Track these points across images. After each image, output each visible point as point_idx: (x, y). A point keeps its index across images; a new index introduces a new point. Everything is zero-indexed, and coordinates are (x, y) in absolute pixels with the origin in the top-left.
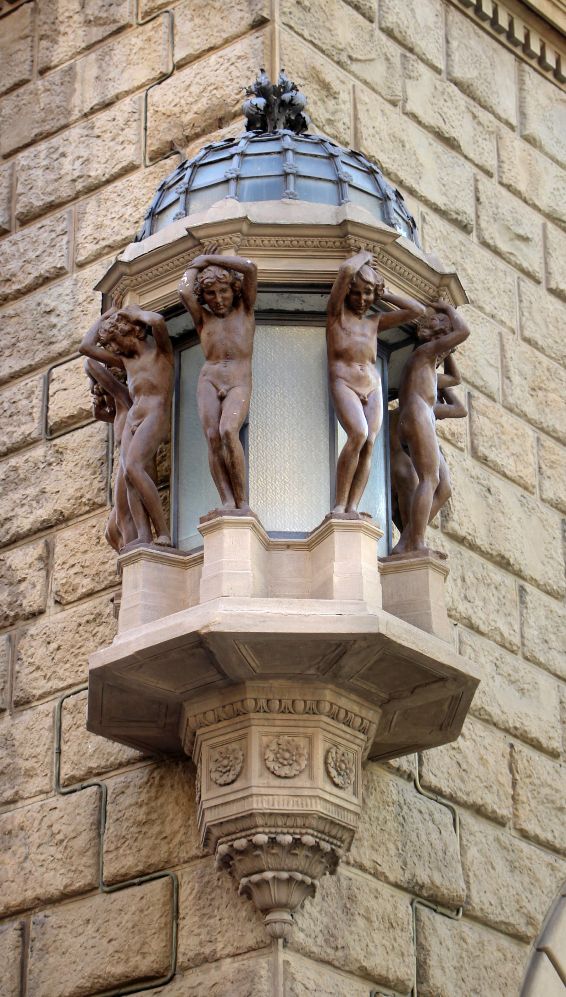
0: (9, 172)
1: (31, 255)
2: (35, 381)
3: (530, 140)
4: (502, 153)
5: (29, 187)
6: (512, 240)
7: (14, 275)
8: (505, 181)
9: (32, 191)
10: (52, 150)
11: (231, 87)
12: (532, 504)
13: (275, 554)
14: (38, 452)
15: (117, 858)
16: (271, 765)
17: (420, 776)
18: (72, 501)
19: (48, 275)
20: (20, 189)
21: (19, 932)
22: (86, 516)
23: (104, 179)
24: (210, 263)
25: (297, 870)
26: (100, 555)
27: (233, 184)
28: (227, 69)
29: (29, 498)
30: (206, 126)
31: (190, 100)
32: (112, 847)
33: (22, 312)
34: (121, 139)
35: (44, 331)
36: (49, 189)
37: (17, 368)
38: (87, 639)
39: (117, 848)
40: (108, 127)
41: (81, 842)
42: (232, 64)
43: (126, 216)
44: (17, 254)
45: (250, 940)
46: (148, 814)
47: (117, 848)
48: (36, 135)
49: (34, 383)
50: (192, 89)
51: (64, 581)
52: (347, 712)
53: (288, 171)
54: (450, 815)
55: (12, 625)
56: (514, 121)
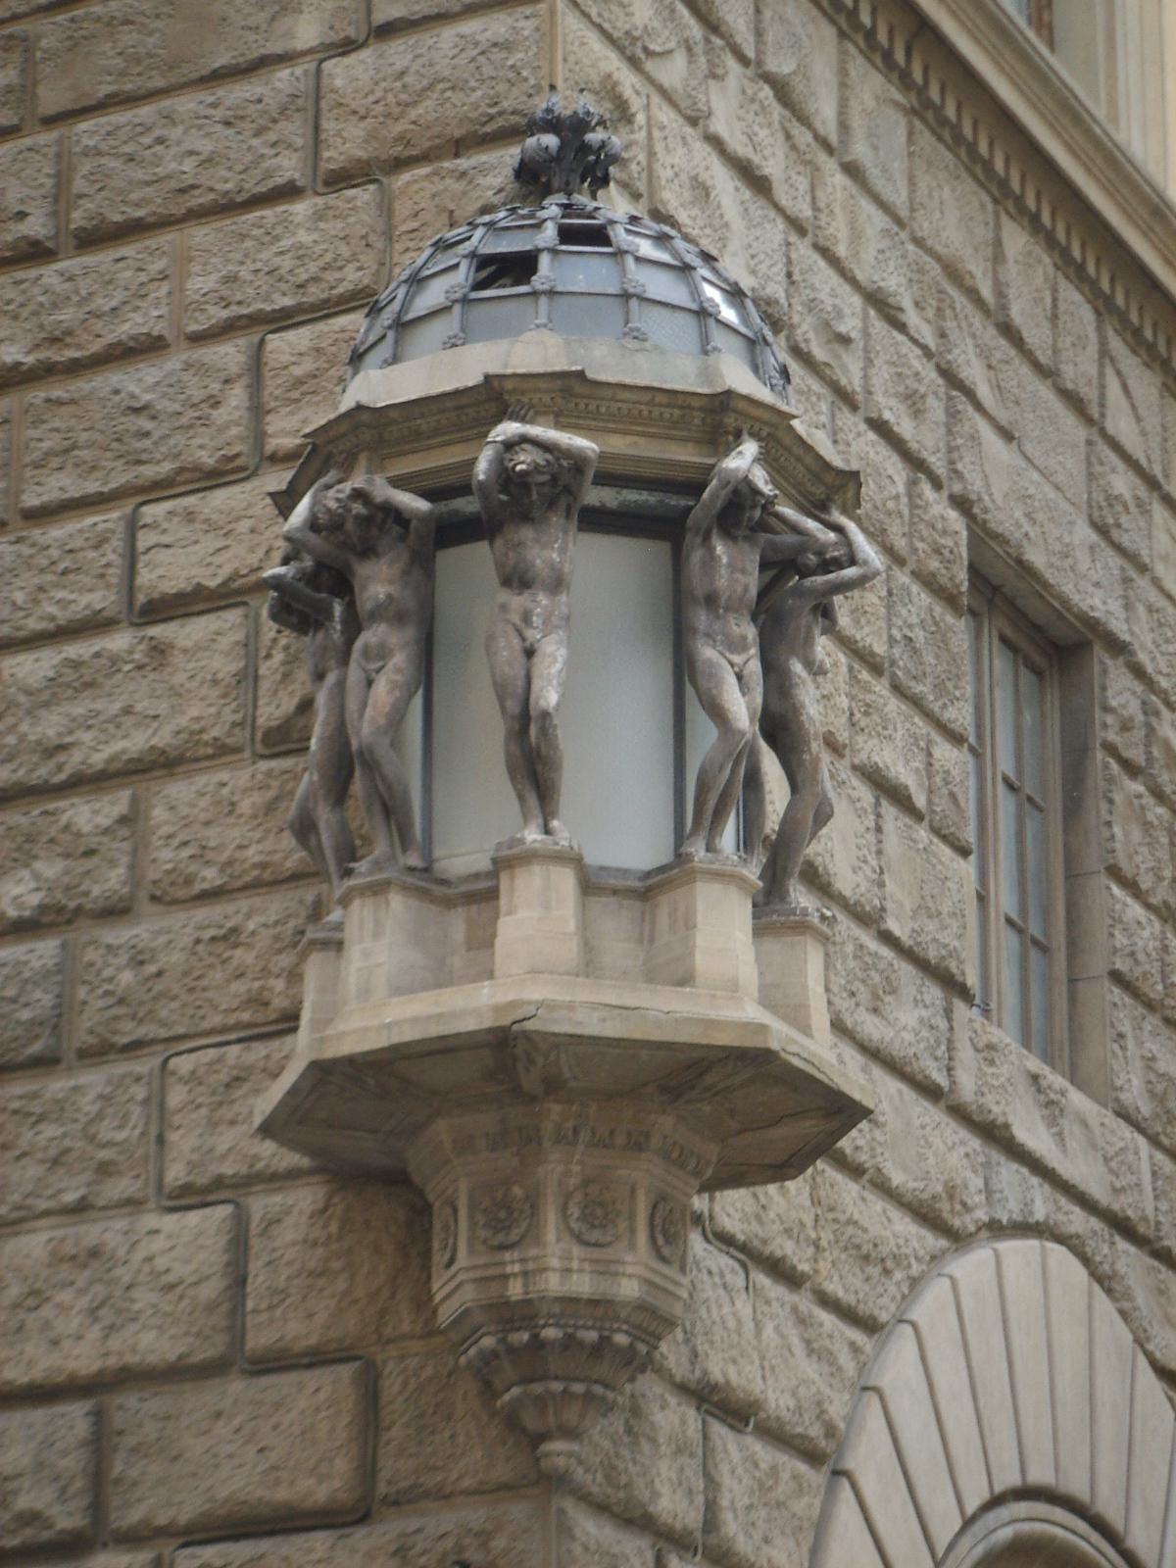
0: (54, 149)
1: (102, 303)
2: (110, 519)
3: (852, 170)
4: (819, 194)
5: (98, 186)
6: (829, 342)
7: (69, 333)
8: (822, 242)
9: (103, 194)
10: (139, 129)
11: (479, 93)
12: (843, 776)
13: (597, 903)
14: (118, 641)
15: (271, 1321)
16: (575, 1226)
17: (711, 1217)
18: (184, 736)
19: (132, 344)
20: (79, 185)
21: (91, 1419)
22: (206, 764)
23: (239, 199)
24: (524, 439)
25: (596, 1382)
26: (236, 833)
27: (543, 300)
28: (473, 60)
29: (101, 718)
30: (430, 148)
31: (404, 97)
32: (263, 1306)
33: (84, 398)
34: (272, 137)
35: (126, 439)
36: (134, 196)
37: (74, 492)
38: (211, 966)
39: (271, 1308)
40: (249, 112)
41: (210, 1290)
42: (482, 53)
43: (282, 271)
44: (75, 298)
45: (502, 1472)
46: (327, 1260)
47: (271, 1308)
48: (107, 96)
49: (109, 525)
50: (409, 79)
51: (169, 866)
52: (682, 1148)
53: (631, 290)
54: (742, 1275)
55: (69, 922)
56: (834, 138)
